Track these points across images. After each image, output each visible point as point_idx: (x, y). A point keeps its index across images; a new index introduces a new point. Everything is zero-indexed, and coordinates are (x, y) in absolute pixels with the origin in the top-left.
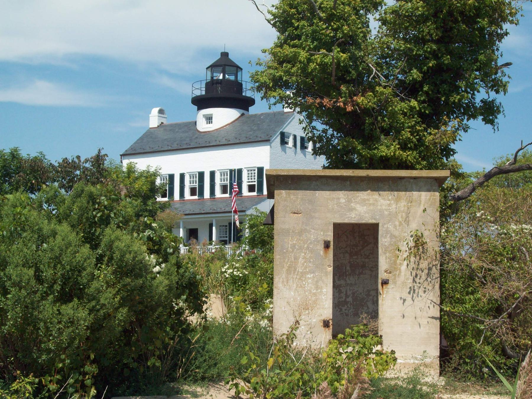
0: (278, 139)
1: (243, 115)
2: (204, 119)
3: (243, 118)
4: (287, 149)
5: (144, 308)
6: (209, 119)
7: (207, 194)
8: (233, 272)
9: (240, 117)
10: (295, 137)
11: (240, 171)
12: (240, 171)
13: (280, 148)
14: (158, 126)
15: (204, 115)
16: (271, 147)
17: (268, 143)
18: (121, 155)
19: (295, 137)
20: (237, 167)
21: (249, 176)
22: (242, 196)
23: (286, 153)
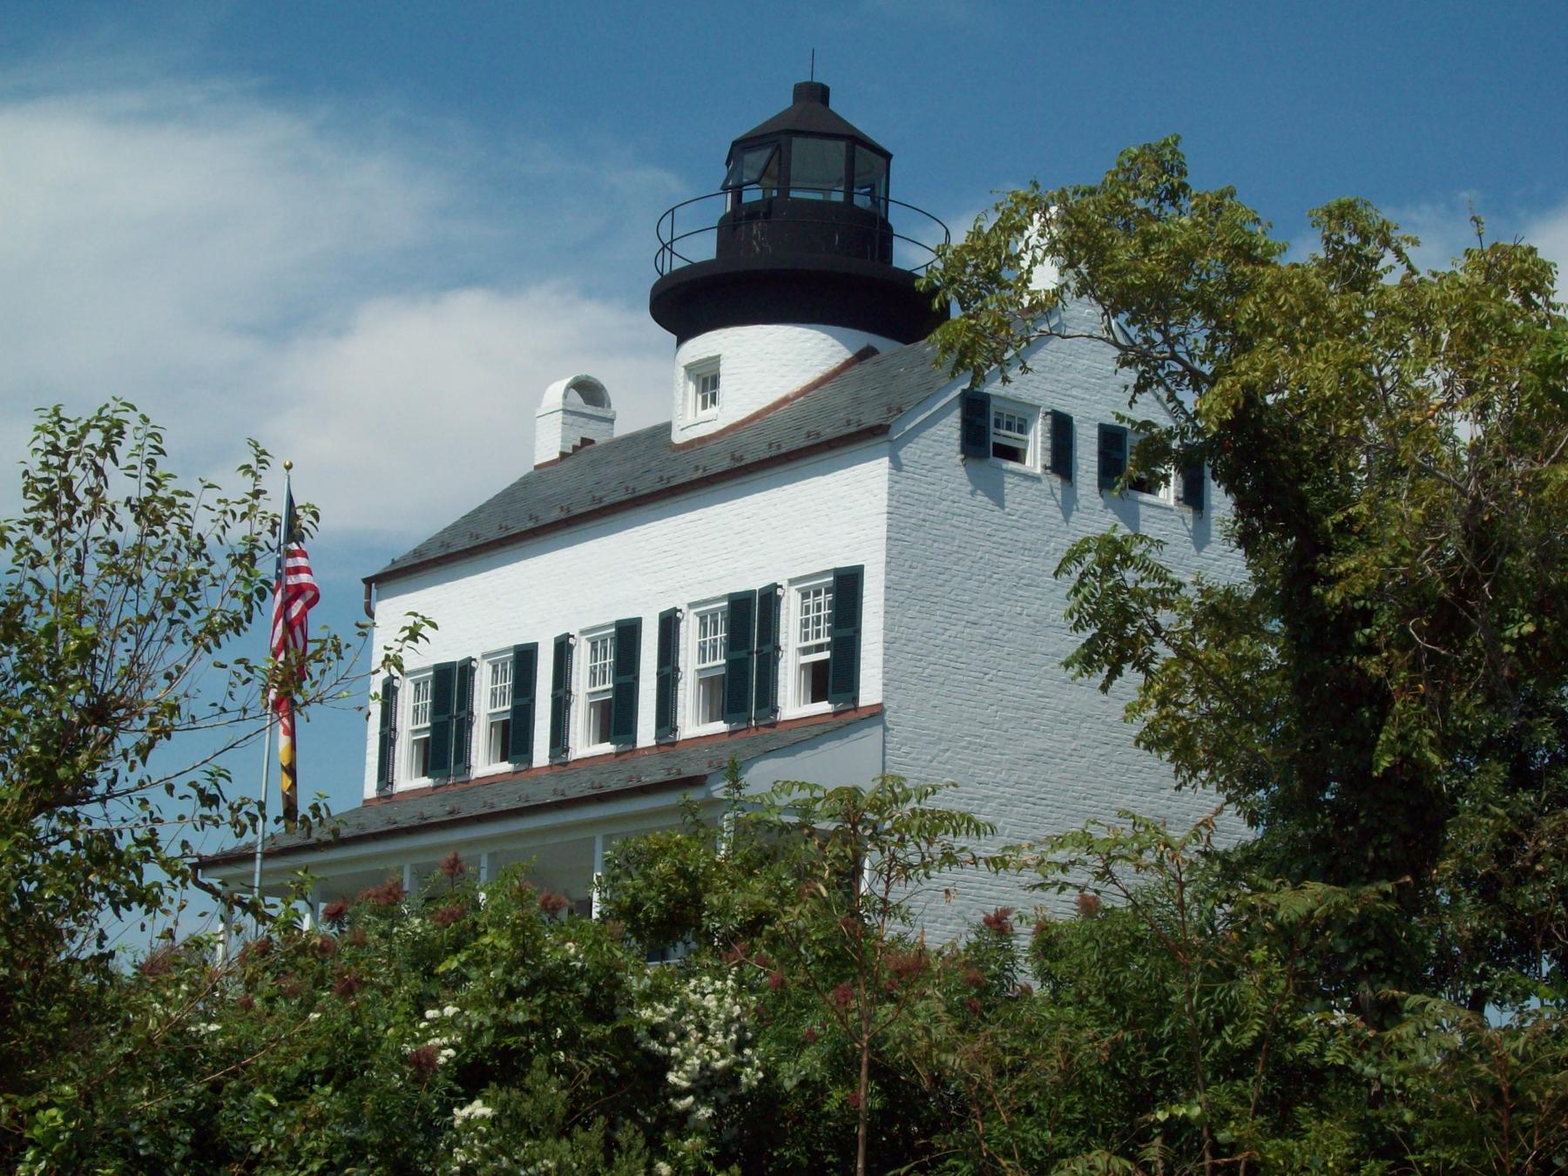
0: (950, 429)
1: (864, 355)
2: (692, 387)
3: (867, 366)
4: (1009, 480)
5: (1389, 1035)
6: (707, 380)
7: (646, 733)
8: (1127, 1044)
9: (847, 365)
10: (1062, 427)
11: (770, 598)
12: (770, 598)
13: (961, 471)
14: (563, 455)
15: (689, 369)
16: (897, 466)
17: (880, 443)
18: (368, 581)
19: (1062, 427)
20: (756, 583)
21: (805, 624)
22: (773, 725)
23: (1000, 503)
